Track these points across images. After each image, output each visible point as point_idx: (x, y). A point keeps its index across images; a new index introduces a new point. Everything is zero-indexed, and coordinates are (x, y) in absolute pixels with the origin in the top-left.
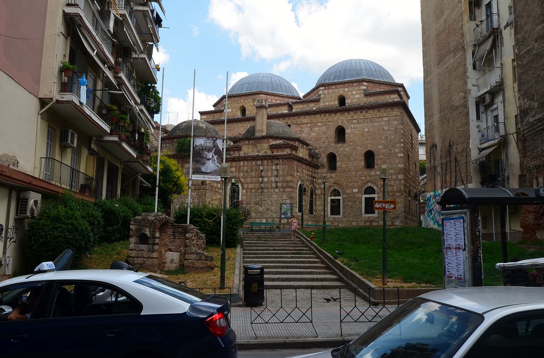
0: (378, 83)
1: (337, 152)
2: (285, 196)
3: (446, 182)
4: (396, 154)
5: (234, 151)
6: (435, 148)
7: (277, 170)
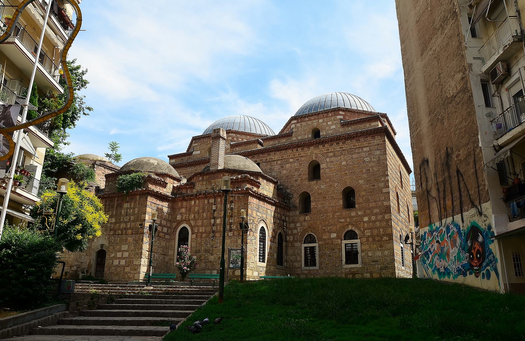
1: (311, 191)
3: (445, 209)
6: (426, 165)
7: (232, 209)
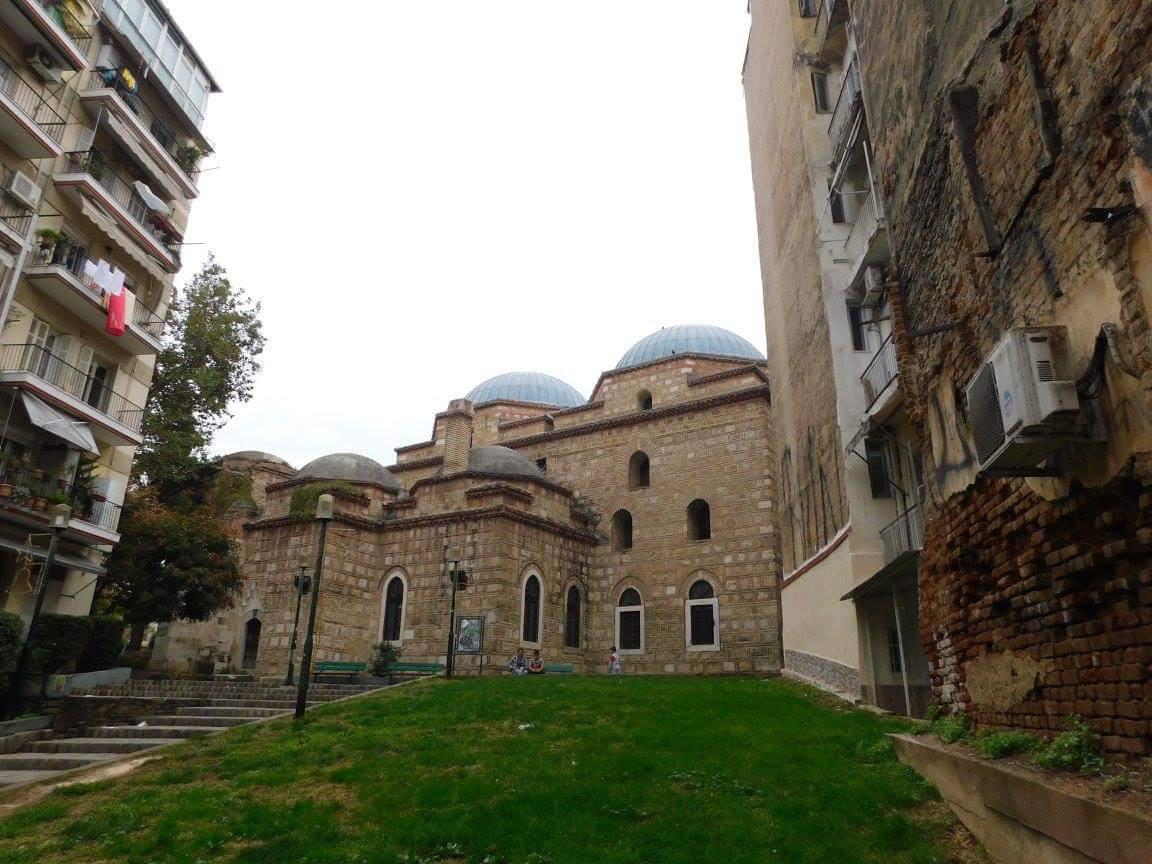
0: (720, 361)
2: (485, 602)
3: (809, 541)
4: (754, 502)
5: (404, 509)
